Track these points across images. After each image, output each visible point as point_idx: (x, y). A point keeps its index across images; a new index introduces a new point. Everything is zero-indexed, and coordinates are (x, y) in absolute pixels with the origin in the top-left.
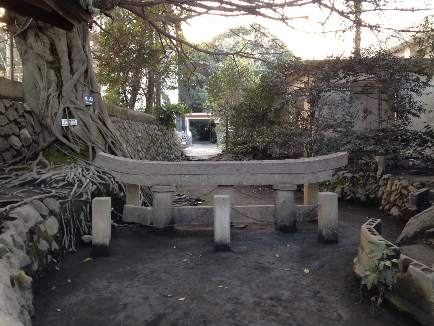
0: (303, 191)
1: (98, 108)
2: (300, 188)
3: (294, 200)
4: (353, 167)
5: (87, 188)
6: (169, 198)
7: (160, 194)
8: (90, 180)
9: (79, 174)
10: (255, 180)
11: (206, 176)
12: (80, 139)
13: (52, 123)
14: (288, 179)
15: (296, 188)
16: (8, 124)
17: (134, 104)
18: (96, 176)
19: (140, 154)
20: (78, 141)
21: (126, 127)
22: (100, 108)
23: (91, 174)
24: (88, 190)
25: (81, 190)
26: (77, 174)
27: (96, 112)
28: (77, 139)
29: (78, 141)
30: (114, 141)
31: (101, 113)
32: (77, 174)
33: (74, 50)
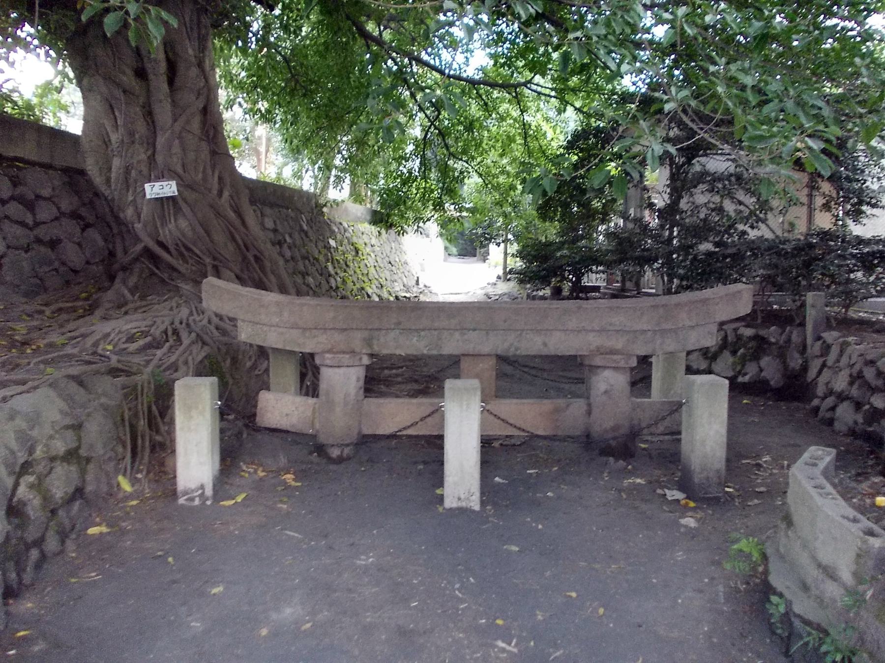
0: (651, 363)
1: (228, 186)
2: (645, 361)
3: (629, 388)
4: (459, 201)
5: (188, 352)
6: (354, 378)
7: (330, 370)
8: (198, 335)
9: (181, 323)
10: (545, 344)
11: (436, 333)
12: (188, 249)
13: (135, 217)
14: (618, 343)
15: (634, 363)
16: (57, 219)
17: (155, 140)
18: (212, 328)
19: (332, 281)
20: (185, 253)
21: (305, 227)
22: (232, 186)
23: (205, 322)
24: (190, 358)
25: (173, 359)
26: (177, 323)
27: (226, 194)
28: (183, 249)
29: (185, 253)
30: (258, 254)
31: (235, 198)
32: (177, 323)
33: (181, 67)
